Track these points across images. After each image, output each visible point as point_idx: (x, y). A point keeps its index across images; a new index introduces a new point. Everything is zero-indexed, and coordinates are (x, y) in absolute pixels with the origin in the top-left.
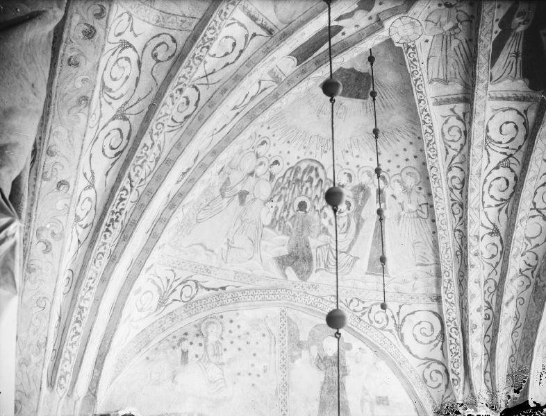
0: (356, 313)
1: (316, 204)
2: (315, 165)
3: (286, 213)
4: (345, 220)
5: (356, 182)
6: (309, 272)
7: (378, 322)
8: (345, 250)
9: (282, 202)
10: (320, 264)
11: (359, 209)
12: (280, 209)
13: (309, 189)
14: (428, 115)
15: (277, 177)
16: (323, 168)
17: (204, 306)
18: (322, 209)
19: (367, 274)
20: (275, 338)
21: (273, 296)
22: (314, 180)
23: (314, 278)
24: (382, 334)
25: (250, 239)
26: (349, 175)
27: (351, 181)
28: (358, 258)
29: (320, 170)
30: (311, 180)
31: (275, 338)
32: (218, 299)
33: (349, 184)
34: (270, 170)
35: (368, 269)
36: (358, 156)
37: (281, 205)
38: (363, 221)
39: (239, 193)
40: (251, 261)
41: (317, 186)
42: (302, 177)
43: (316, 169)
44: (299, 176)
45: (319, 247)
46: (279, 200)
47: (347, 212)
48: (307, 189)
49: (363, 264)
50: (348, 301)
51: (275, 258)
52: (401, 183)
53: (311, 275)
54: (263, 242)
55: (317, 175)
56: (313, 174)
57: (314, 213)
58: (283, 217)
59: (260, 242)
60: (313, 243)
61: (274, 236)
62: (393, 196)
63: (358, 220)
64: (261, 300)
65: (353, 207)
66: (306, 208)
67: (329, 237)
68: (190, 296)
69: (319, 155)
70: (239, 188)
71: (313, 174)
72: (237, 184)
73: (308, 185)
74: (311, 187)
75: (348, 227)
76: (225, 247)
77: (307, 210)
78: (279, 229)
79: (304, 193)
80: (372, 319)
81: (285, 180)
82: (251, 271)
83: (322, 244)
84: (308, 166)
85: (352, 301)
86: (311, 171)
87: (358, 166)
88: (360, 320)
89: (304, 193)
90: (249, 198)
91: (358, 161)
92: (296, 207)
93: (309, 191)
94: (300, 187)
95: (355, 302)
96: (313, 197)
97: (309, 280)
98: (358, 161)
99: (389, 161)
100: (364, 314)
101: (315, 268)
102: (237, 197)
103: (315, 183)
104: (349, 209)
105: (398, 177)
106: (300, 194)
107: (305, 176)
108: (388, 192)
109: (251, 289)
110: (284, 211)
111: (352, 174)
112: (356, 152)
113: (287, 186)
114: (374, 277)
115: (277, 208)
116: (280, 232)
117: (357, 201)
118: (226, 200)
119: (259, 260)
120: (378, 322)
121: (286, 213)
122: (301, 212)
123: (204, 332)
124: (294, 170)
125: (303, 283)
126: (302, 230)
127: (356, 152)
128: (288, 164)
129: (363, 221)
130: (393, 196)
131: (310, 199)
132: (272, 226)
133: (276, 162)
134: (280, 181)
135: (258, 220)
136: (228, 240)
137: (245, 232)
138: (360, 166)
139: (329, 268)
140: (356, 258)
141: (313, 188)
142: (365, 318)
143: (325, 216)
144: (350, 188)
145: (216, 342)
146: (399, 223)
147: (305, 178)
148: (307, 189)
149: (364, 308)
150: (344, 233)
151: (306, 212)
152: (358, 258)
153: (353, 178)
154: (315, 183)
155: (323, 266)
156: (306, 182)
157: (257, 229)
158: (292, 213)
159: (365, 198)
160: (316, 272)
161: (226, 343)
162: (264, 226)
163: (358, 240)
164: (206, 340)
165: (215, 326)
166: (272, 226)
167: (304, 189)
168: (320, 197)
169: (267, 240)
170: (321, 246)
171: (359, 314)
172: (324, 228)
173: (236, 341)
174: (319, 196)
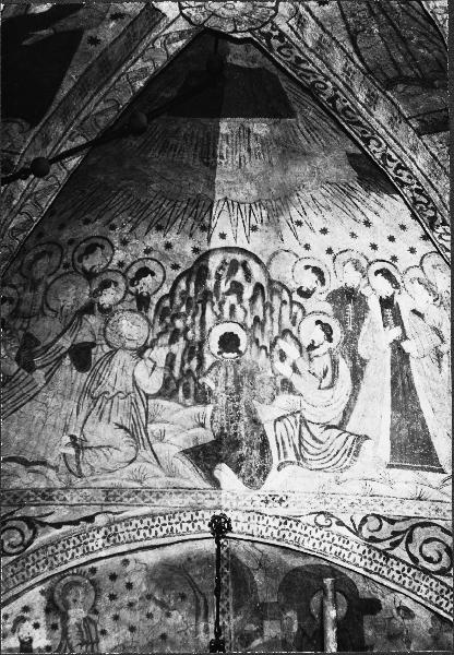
0: (378, 546)
1: (258, 335)
2: (240, 258)
3: (194, 363)
4: (326, 361)
5: (333, 284)
6: (263, 472)
7: (429, 560)
8: (336, 423)
9: (181, 343)
10: (285, 454)
11: (351, 339)
12: (178, 358)
13: (238, 308)
14: (399, 167)
15: (155, 300)
16: (258, 261)
17: (50, 559)
18: (273, 345)
19: (390, 466)
20: (206, 601)
21: (190, 525)
22: (246, 289)
23: (275, 481)
24: (442, 583)
25: (121, 427)
26: (317, 271)
27: (323, 282)
28: (367, 437)
29: (252, 265)
30: (237, 289)
31: (206, 601)
32: (78, 542)
33: (320, 288)
34: (132, 289)
35: (392, 459)
36: (324, 231)
37: (179, 348)
38: (364, 363)
39: (69, 351)
40: (133, 466)
41: (253, 299)
42: (217, 286)
43: (244, 264)
44: (211, 284)
45: (279, 419)
46: (172, 341)
47: (327, 345)
48: (232, 308)
49: (379, 448)
50: (357, 523)
51: (185, 452)
52: (429, 286)
53: (270, 476)
54: (151, 427)
55: (248, 275)
56: (239, 276)
57: (259, 353)
58: (189, 371)
59: (145, 428)
60: (266, 414)
61: (178, 411)
62: (414, 311)
63: (354, 361)
64: (164, 537)
65: (337, 334)
66: (238, 345)
67: (297, 398)
68: (21, 544)
69: (241, 234)
70: (66, 343)
71: (239, 276)
72: (59, 336)
73: (232, 299)
74: (240, 300)
75: (334, 376)
76: (71, 451)
77: (242, 348)
78: (186, 396)
79: (226, 315)
80: (417, 554)
81: (178, 301)
82: (140, 481)
83: (285, 413)
84: (224, 262)
85: (364, 520)
86: (233, 271)
87: (330, 251)
88: (388, 557)
89: (226, 315)
90: (98, 353)
91: (327, 241)
92: (215, 348)
93: (239, 312)
94: (216, 307)
95: (374, 523)
96: (250, 322)
97: (263, 488)
98: (327, 241)
99: (392, 239)
100: (395, 545)
101: (276, 462)
102: (67, 361)
103: (248, 292)
104: (330, 340)
105: (417, 273)
106: (219, 319)
107: (223, 282)
108: (404, 303)
109: (145, 516)
110: (190, 359)
111: (324, 269)
112: (318, 223)
113: (183, 309)
114: (410, 472)
115: (171, 358)
116: (189, 402)
117: (343, 324)
118: (40, 373)
119: (153, 460)
120: (429, 560)
121: (194, 363)
122: (231, 355)
123: (59, 603)
124: (194, 278)
125: (253, 494)
126: (239, 390)
127: (318, 223)
128: (175, 267)
129: (364, 363)
130: (414, 311)
131: (243, 326)
132: (167, 391)
133: (145, 272)
134: (167, 303)
135: (130, 389)
136: (72, 437)
137: (106, 416)
138: (336, 251)
139: (305, 460)
140: (361, 438)
141: (246, 304)
142: (400, 552)
143: (283, 356)
144: (324, 296)
145: (84, 619)
146: (440, 367)
147: (224, 287)
148: (232, 308)
149: (395, 534)
150: (329, 387)
151: (240, 353)
152: (367, 437)
153: (326, 276)
154: (248, 292)
155: (292, 457)
156: (228, 293)
157: (134, 404)
158: (209, 360)
159: (359, 319)
160: (279, 469)
161: (106, 621)
162: (147, 396)
163: (359, 402)
164: (65, 618)
165: (81, 591)
166: (167, 391)
167: (226, 308)
168: (265, 320)
169: (162, 421)
170: (284, 417)
171: (386, 545)
172: (285, 381)
173: (125, 614)
174: (261, 318)
